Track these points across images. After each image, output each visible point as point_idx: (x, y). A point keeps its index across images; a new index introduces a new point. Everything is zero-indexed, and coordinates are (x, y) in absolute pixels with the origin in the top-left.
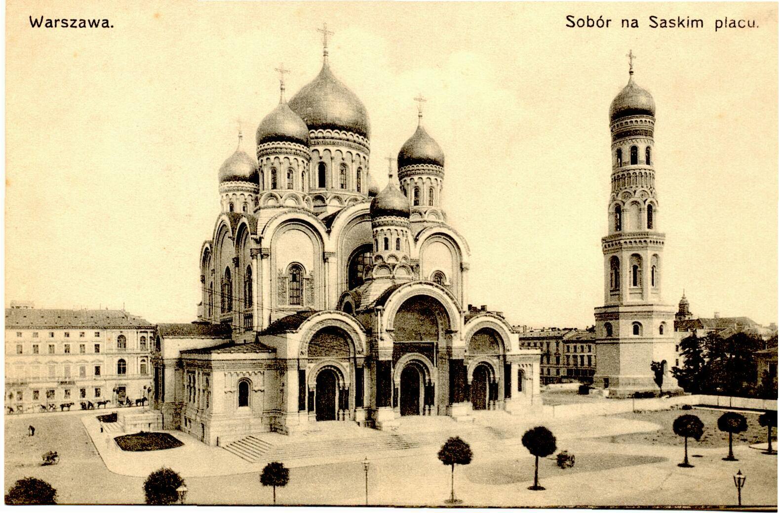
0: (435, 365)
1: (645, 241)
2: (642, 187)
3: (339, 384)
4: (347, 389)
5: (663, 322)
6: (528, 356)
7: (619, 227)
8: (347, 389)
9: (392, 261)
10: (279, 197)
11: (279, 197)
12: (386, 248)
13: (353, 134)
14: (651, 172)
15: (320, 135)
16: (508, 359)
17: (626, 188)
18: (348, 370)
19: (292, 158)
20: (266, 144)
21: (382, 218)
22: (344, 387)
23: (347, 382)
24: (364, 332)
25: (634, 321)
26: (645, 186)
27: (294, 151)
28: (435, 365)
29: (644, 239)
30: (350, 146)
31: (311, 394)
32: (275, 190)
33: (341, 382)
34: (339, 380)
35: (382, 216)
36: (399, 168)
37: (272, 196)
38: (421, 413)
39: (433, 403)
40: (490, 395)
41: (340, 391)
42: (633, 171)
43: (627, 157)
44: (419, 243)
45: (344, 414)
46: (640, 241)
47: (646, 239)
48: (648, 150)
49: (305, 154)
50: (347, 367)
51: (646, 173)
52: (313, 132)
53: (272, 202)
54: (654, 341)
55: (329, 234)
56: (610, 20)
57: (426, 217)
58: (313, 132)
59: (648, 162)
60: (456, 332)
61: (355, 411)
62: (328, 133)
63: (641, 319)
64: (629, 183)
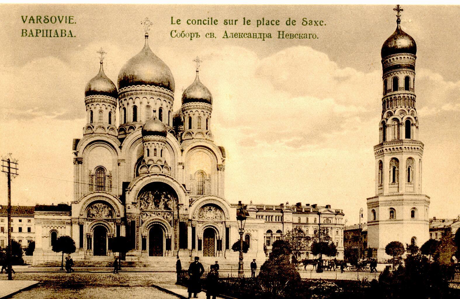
0: (172, 226)
1: (401, 148)
2: (401, 107)
3: (216, 236)
4: (220, 239)
5: (414, 208)
6: (254, 224)
7: (384, 139)
8: (220, 239)
9: (150, 163)
10: (92, 127)
11: (92, 127)
12: (155, 155)
13: (159, 87)
14: (413, 96)
15: (133, 89)
16: (228, 224)
17: (389, 109)
18: (222, 229)
19: (200, 110)
20: (186, 104)
21: (148, 136)
22: (168, 236)
23: (221, 235)
24: (121, 204)
25: (391, 207)
26: (404, 107)
27: (102, 100)
28: (172, 226)
29: (400, 147)
30: (152, 94)
31: (200, 241)
32: (190, 130)
33: (218, 235)
34: (216, 234)
35: (148, 135)
36: (183, 104)
37: (189, 133)
38: (164, 255)
39: (221, 250)
40: (217, 248)
41: (217, 240)
42: (394, 96)
43: (390, 86)
44: (185, 153)
45: (219, 253)
46: (393, 149)
47: (401, 146)
48: (407, 79)
49: (111, 101)
50: (112, 225)
51: (408, 97)
52: (129, 87)
53: (189, 137)
54: (404, 222)
55: (121, 149)
56: (237, 20)
57: (193, 136)
58: (129, 87)
59: (407, 87)
60: (182, 205)
61: (225, 251)
62: (129, 88)
63: (394, 205)
64: (391, 105)
